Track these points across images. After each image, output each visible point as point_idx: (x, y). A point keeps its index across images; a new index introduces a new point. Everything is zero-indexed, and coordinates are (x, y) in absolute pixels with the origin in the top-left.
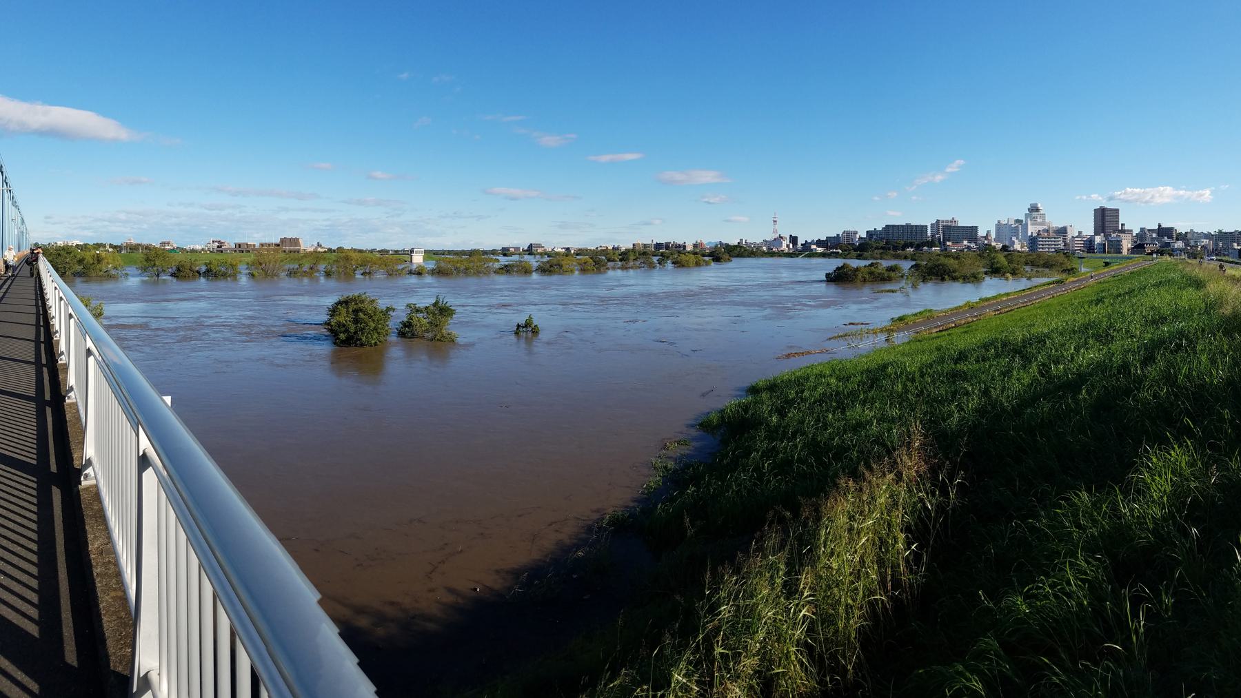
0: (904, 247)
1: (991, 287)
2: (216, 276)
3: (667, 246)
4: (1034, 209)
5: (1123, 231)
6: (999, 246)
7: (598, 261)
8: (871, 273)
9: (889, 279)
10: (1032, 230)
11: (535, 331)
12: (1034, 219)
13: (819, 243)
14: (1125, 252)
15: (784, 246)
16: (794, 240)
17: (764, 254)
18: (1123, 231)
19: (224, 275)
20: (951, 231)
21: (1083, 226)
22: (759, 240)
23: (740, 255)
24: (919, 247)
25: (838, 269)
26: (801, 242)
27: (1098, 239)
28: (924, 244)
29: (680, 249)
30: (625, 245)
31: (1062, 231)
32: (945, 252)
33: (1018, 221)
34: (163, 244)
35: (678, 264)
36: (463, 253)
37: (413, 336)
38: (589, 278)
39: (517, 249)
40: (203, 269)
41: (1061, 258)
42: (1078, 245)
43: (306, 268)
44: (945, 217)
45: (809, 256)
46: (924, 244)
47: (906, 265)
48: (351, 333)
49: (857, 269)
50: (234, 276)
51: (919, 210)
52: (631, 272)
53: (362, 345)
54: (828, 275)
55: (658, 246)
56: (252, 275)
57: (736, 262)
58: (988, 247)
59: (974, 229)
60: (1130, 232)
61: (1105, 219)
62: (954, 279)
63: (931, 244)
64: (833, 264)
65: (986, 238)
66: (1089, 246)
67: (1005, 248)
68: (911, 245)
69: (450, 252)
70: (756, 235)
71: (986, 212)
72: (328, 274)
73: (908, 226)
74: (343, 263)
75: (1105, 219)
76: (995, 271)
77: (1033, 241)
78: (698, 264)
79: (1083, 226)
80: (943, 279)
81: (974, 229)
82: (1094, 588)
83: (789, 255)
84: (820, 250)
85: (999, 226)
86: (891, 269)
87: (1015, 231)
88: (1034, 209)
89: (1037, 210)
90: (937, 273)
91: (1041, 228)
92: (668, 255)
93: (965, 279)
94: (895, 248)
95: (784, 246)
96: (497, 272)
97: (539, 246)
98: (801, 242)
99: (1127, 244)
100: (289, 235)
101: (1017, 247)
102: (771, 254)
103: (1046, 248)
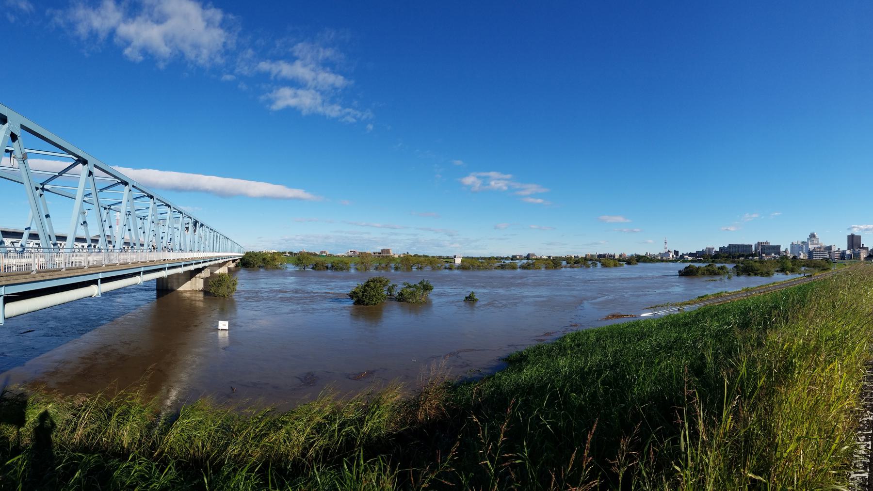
0: (739, 257)
1: (780, 278)
2: (336, 269)
3: (604, 256)
4: (813, 236)
5: (863, 248)
6: (792, 256)
7: (554, 263)
8: (708, 270)
9: (718, 274)
10: (811, 247)
11: (475, 300)
12: (812, 241)
13: (690, 255)
14: (862, 259)
15: (671, 256)
16: (676, 253)
17: (658, 261)
18: (863, 248)
19: (341, 269)
20: (765, 248)
21: (841, 245)
22: (656, 253)
23: (645, 261)
24: (747, 257)
25: (686, 268)
26: (680, 254)
27: (848, 252)
28: (750, 255)
29: (612, 257)
30: (582, 255)
31: (829, 248)
32: (761, 262)
33: (804, 243)
34: (322, 252)
35: (604, 265)
36: (485, 258)
37: (404, 300)
38: (549, 272)
39: (521, 256)
40: (330, 266)
41: (824, 263)
42: (837, 256)
43: (383, 265)
44: (763, 240)
45: (683, 262)
46: (750, 255)
47: (730, 266)
48: (365, 301)
49: (699, 268)
50: (348, 269)
51: (748, 236)
52: (576, 269)
53: (367, 304)
54: (680, 272)
55: (600, 256)
56: (357, 269)
57: (640, 265)
58: (786, 257)
59: (778, 247)
60: (867, 248)
61: (854, 241)
62: (756, 274)
63: (754, 255)
64: (682, 266)
65: (785, 252)
66: (843, 256)
67: (795, 257)
68: (743, 256)
69: (482, 258)
70: (654, 250)
71: (785, 237)
72: (396, 269)
73: (743, 245)
74: (362, 260)
75: (854, 241)
76: (783, 270)
77: (810, 253)
78: (615, 265)
79: (841, 245)
80: (749, 275)
81: (778, 247)
82: (205, 396)
83: (672, 261)
84: (690, 258)
85: (792, 245)
86: (722, 268)
87: (801, 248)
88: (813, 236)
89: (814, 236)
90: (747, 271)
91: (816, 246)
92: (606, 261)
93: (762, 275)
94: (734, 257)
95: (671, 256)
96: (496, 268)
97: (533, 255)
98: (680, 254)
99: (863, 255)
100: (386, 248)
101: (802, 257)
102: (662, 260)
103: (817, 258)
